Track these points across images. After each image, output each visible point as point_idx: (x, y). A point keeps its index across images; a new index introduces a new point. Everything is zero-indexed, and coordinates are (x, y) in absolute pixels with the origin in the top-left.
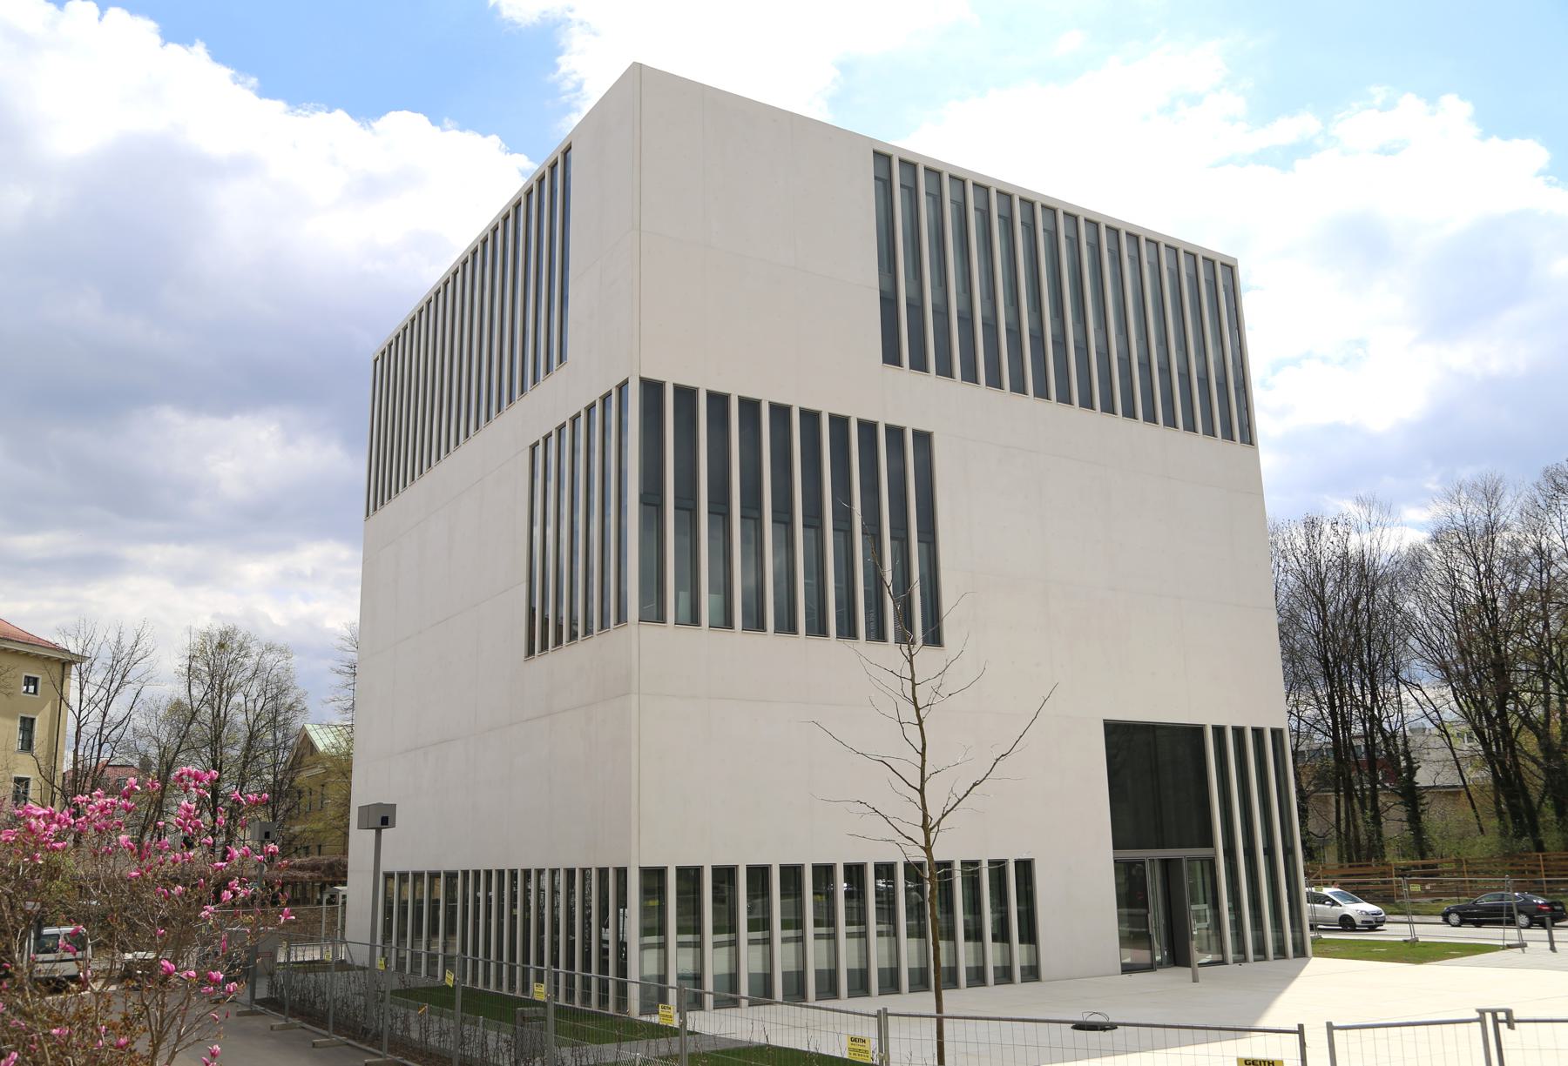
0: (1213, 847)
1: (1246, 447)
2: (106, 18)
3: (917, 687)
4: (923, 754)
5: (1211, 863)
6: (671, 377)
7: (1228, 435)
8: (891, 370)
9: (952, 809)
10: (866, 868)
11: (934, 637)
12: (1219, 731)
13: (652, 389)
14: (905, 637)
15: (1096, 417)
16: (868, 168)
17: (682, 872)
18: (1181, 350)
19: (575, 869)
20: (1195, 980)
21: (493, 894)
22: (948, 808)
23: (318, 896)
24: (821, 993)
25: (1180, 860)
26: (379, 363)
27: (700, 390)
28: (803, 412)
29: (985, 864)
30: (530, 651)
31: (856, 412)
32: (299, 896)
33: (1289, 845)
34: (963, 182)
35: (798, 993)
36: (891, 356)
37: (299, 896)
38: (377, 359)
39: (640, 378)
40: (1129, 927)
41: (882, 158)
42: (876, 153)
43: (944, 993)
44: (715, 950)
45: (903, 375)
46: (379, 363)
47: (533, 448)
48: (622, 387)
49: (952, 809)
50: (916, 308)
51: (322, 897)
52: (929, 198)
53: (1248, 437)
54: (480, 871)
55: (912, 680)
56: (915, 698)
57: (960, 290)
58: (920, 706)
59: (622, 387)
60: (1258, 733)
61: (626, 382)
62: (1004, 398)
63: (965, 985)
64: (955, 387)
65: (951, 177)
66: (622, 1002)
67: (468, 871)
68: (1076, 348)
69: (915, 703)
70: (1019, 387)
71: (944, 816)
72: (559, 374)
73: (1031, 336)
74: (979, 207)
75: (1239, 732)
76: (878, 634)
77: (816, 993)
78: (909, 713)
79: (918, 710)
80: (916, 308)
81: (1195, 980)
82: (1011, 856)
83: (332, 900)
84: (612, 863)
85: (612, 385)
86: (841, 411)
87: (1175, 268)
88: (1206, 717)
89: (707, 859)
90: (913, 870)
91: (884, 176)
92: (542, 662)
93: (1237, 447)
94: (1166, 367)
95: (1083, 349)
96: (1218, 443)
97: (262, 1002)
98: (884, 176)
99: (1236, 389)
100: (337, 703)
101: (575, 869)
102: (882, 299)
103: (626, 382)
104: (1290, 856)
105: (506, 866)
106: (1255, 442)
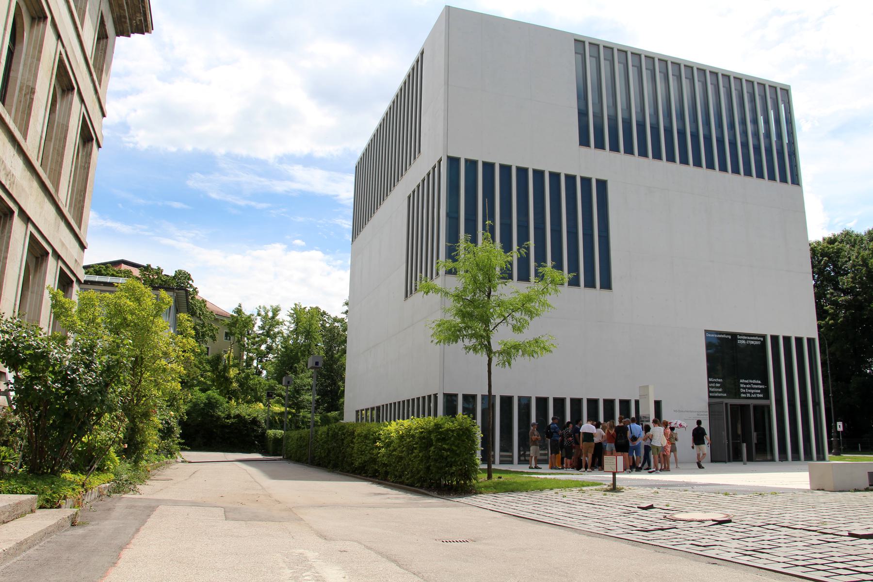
1: (795, 187)
5: (769, 407)
8: (584, 149)
10: (631, 402)
11: (607, 284)
12: (775, 339)
15: (741, 178)
17: (589, 401)
21: (432, 405)
25: (749, 406)
27: (529, 169)
28: (582, 179)
30: (406, 296)
34: (776, 88)
41: (580, 43)
42: (575, 40)
52: (661, 74)
53: (796, 180)
54: (456, 395)
60: (799, 340)
64: (621, 157)
65: (710, 72)
67: (414, 399)
68: (766, 150)
75: (787, 339)
86: (555, 170)
87: (775, 97)
88: (769, 332)
93: (789, 187)
96: (777, 185)
97: (285, 459)
102: (579, 113)
104: (817, 407)
106: (800, 184)
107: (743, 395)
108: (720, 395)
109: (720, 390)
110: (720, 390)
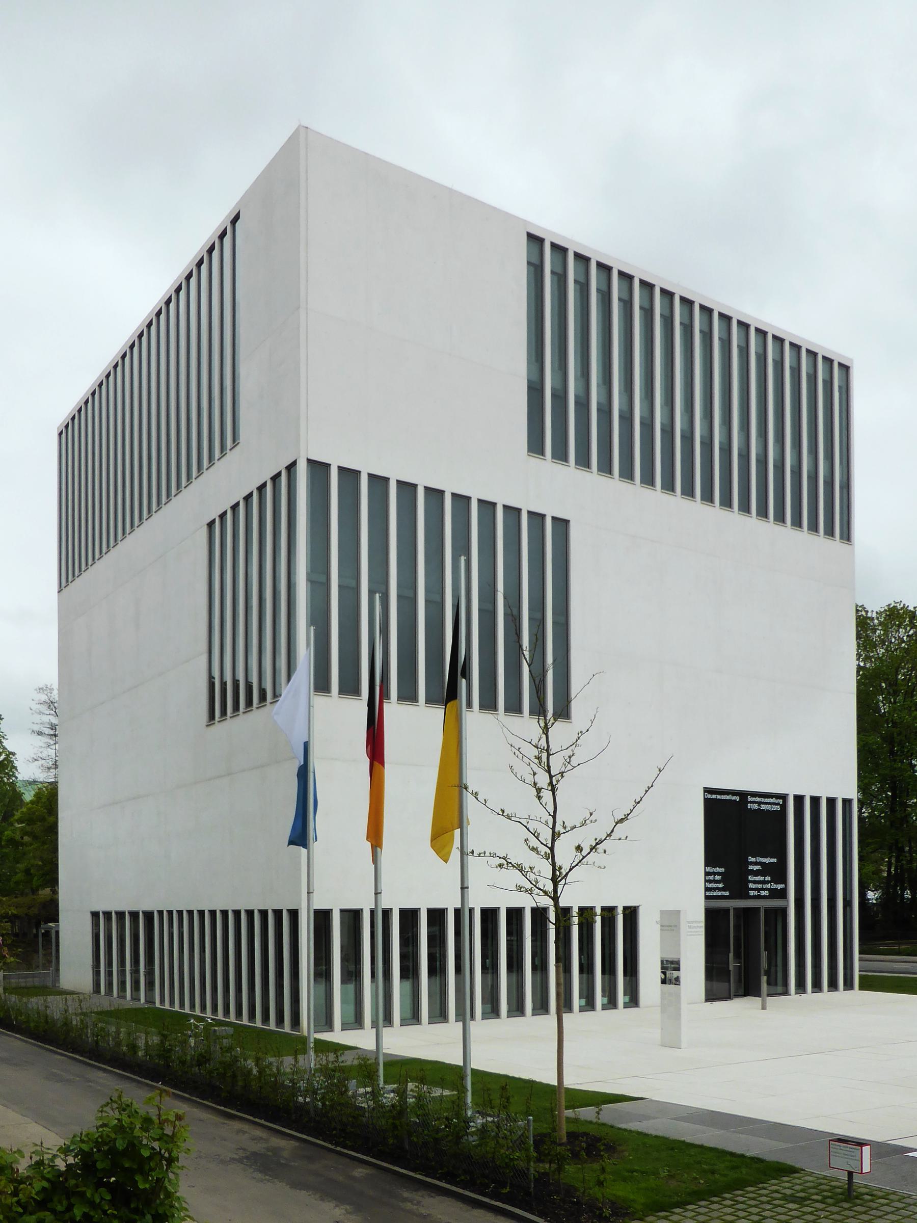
0: (786, 898)
2: (238, 211)
3: (551, 757)
4: (554, 817)
5: (784, 911)
6: (336, 459)
7: (830, 532)
9: (577, 865)
11: (563, 712)
13: (319, 469)
14: (539, 709)
16: (520, 253)
17: (582, 910)
18: (761, 437)
19: (216, 910)
20: (764, 1008)
22: (573, 865)
23: (34, 931)
24: (433, 1017)
26: (64, 435)
29: (620, 910)
30: (212, 716)
31: (501, 498)
32: (17, 931)
33: (848, 899)
35: (356, 1022)
36: (536, 446)
37: (17, 931)
38: (62, 432)
39: (308, 459)
40: (436, 976)
41: (535, 241)
43: (564, 1015)
44: (402, 980)
45: (546, 466)
46: (64, 435)
47: (211, 525)
48: (291, 467)
49: (577, 865)
50: (560, 397)
51: (37, 932)
55: (548, 750)
56: (549, 767)
57: (579, 373)
58: (553, 774)
59: (291, 467)
61: (294, 464)
62: (803, 536)
63: (578, 1010)
64: (592, 479)
66: (296, 1021)
67: (162, 911)
69: (549, 771)
70: (648, 480)
71: (570, 870)
72: (233, 456)
73: (791, 471)
74: (601, 288)
75: (815, 801)
76: (514, 707)
77: (429, 1017)
78: (543, 779)
79: (551, 777)
80: (560, 397)
81: (764, 1008)
82: (620, 903)
83: (47, 934)
84: (285, 906)
85: (281, 466)
89: (206, 907)
90: (539, 914)
91: (535, 260)
92: (219, 728)
93: (835, 545)
94: (797, 471)
95: (814, 478)
98: (535, 260)
99: (841, 488)
100: (41, 762)
101: (216, 910)
103: (294, 464)
105: (270, 905)
107: (752, 893)
108: (720, 893)
109: (721, 886)
110: (721, 886)
